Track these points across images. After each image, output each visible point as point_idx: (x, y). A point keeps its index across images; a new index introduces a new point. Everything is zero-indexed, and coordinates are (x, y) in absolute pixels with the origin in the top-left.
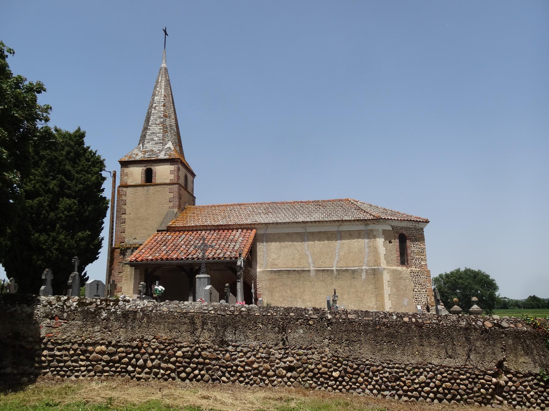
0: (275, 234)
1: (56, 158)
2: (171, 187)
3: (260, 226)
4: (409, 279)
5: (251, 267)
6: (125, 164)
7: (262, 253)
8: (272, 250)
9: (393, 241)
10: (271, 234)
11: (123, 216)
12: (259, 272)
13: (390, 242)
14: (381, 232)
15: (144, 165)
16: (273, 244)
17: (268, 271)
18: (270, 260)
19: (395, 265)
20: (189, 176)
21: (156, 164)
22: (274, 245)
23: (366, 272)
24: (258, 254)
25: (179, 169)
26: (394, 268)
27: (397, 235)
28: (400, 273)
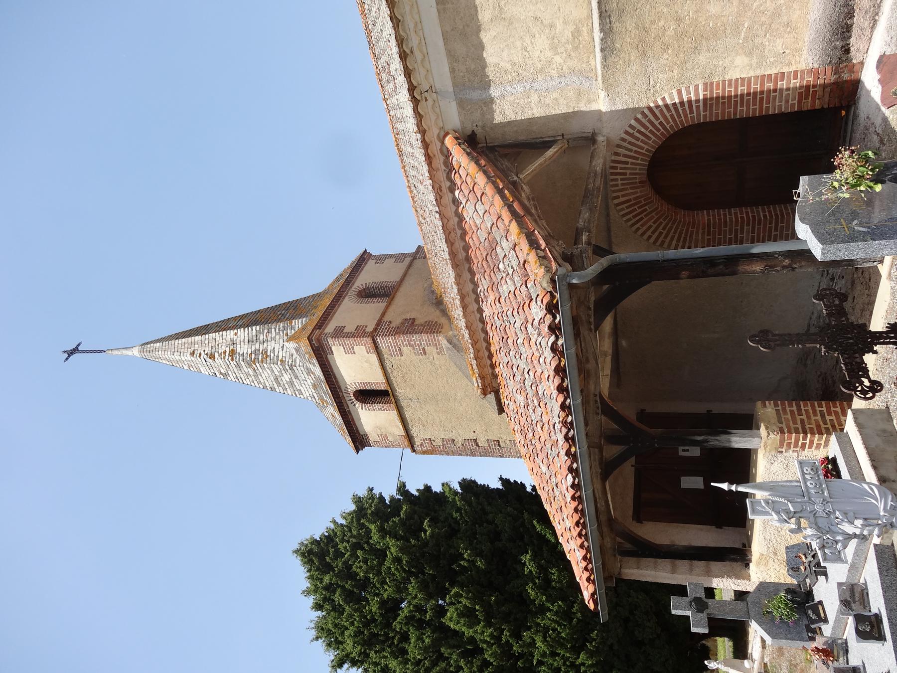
0: (451, 55)
1: (358, 633)
2: (385, 352)
3: (429, 121)
5: (591, 139)
6: (359, 441)
7: (535, 97)
8: (518, 58)
10: (453, 70)
11: (482, 442)
12: (613, 100)
15: (351, 406)
16: (491, 55)
17: (605, 67)
18: (558, 59)
19: (891, 309)
20: (364, 279)
21: (341, 384)
22: (498, 53)
24: (538, 112)
25: (339, 333)
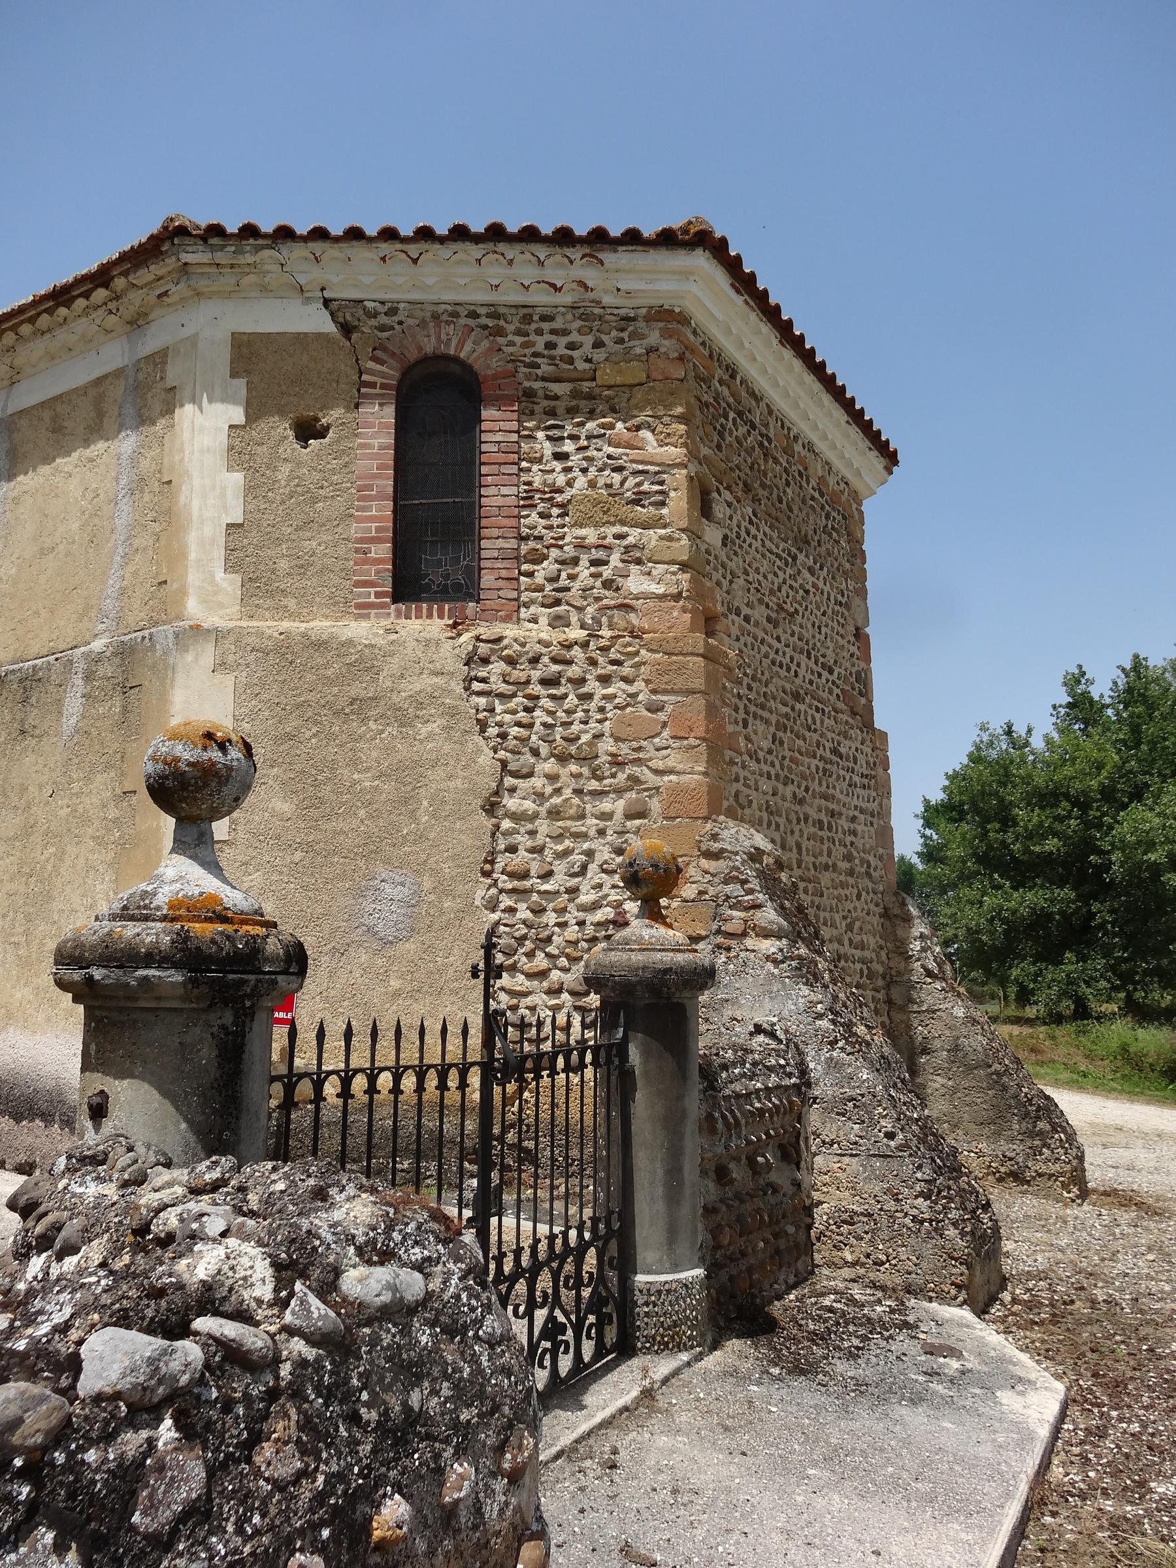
4: (452, 712)
9: (332, 416)
13: (307, 431)
14: (223, 356)
23: (89, 677)
26: (320, 626)
27: (386, 372)
28: (365, 663)
